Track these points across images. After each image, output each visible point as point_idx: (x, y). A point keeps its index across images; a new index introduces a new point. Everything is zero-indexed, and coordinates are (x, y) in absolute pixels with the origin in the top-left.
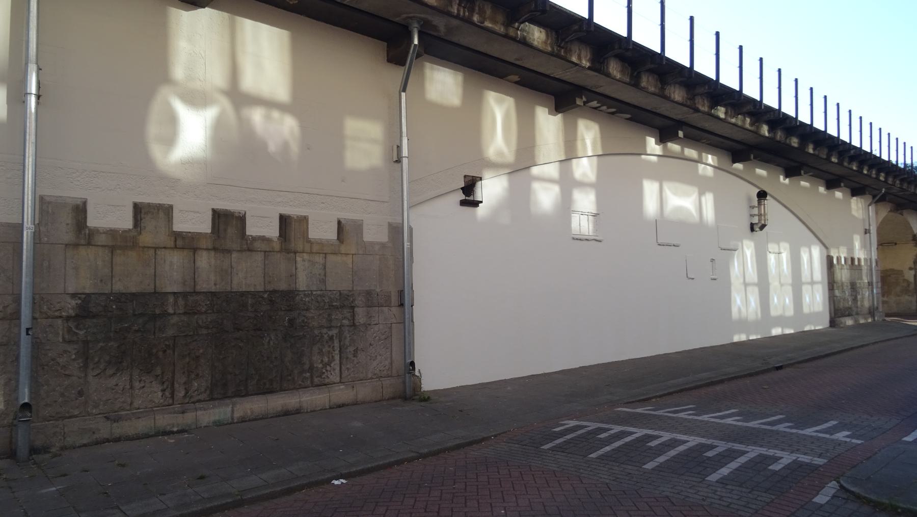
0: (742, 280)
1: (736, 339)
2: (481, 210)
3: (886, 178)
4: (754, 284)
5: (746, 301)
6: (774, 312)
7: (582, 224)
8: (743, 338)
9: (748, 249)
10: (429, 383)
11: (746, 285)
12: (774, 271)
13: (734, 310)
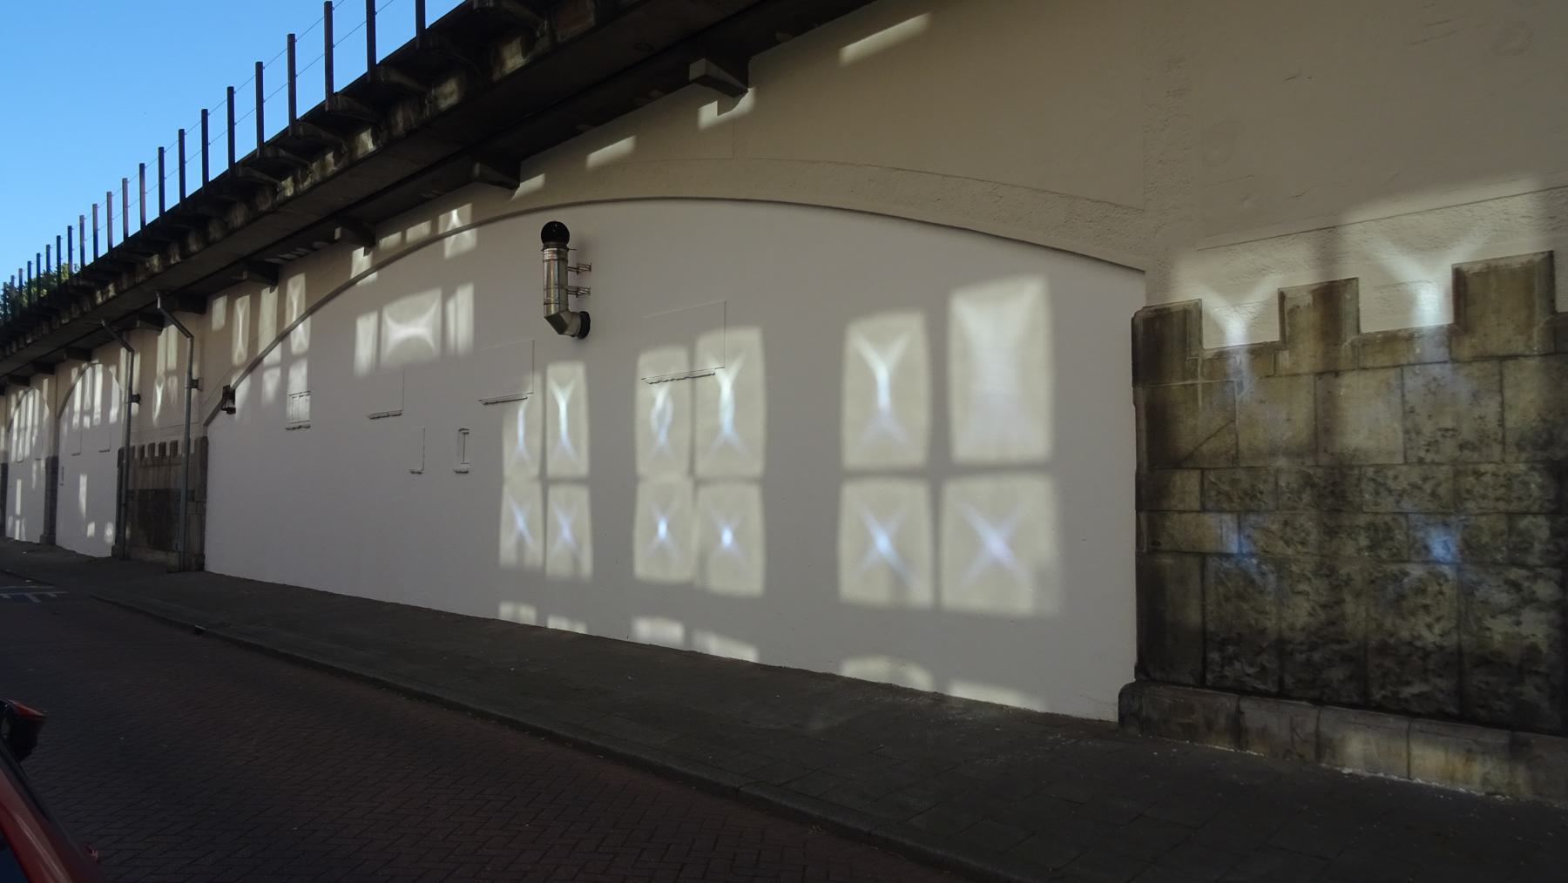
0: (534, 470)
1: (506, 612)
2: (237, 415)
3: (165, 258)
4: (577, 481)
5: (546, 526)
6: (644, 567)
7: (300, 407)
8: (527, 615)
9: (564, 392)
10: (214, 564)
11: (546, 481)
12: (662, 438)
13: (507, 543)
